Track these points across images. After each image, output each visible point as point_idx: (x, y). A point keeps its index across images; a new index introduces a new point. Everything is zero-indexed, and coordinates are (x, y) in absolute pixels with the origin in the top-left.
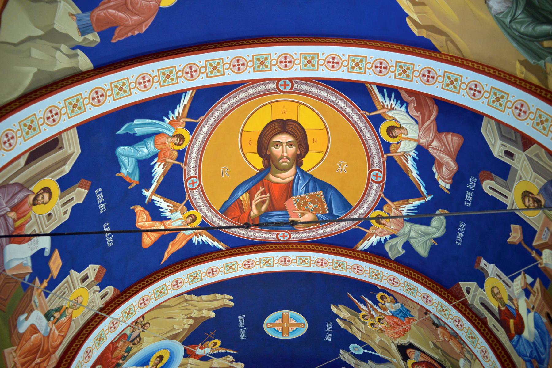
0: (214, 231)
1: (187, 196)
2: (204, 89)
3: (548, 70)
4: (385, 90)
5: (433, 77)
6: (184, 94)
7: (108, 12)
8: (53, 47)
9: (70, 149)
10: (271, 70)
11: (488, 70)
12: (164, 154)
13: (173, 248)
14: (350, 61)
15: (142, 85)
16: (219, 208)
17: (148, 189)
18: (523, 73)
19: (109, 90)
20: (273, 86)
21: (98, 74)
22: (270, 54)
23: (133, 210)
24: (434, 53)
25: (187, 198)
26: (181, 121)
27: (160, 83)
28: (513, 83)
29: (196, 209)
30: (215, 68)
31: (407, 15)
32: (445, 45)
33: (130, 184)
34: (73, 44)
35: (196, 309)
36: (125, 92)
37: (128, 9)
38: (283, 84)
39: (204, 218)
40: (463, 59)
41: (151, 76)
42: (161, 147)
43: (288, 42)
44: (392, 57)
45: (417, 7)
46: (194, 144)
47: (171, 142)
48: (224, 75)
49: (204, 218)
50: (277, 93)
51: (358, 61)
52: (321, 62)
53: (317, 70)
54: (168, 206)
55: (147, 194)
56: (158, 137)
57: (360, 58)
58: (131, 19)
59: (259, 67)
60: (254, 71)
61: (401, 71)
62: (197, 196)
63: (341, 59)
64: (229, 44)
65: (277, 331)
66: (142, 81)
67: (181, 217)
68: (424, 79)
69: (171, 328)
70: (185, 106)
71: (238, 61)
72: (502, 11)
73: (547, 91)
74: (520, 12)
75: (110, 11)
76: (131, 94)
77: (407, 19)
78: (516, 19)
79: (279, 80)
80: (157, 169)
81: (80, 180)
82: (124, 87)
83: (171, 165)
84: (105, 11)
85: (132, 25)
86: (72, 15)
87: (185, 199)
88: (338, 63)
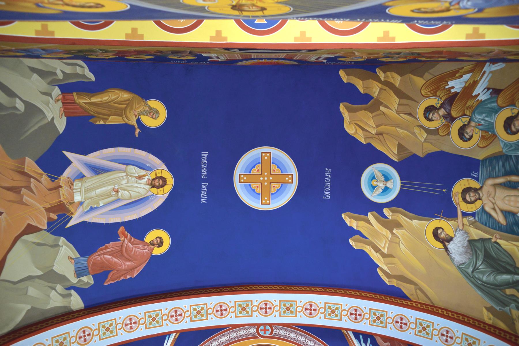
2: (186, 332)
3: (514, 317)
4: (361, 336)
5: (406, 324)
6: (168, 337)
7: (104, 257)
8: (49, 287)
10: (252, 316)
11: (457, 317)
14: (327, 308)
15: (129, 327)
18: (491, 319)
19: (96, 329)
20: (253, 330)
21: (88, 314)
22: (252, 301)
24: (405, 300)
27: (146, 325)
28: (482, 329)
30: (199, 313)
31: (378, 266)
32: (415, 293)
34: (68, 285)
36: (112, 332)
37: (122, 255)
38: (263, 329)
40: (433, 306)
41: (138, 318)
43: (268, 290)
44: (365, 305)
45: (385, 259)
48: (207, 319)
50: (257, 337)
51: (334, 309)
52: (299, 309)
53: (296, 316)
57: (336, 306)
58: (125, 265)
59: (240, 312)
60: (236, 317)
61: (375, 318)
63: (318, 307)
64: (213, 290)
65: (254, 190)
66: (128, 322)
68: (397, 326)
71: (221, 306)
72: (464, 262)
73: (516, 336)
74: (480, 263)
75: (105, 256)
76: (117, 335)
77: (378, 270)
78: (477, 269)
79: (259, 325)
82: (111, 328)
84: (102, 257)
86: (71, 258)
88: (315, 310)
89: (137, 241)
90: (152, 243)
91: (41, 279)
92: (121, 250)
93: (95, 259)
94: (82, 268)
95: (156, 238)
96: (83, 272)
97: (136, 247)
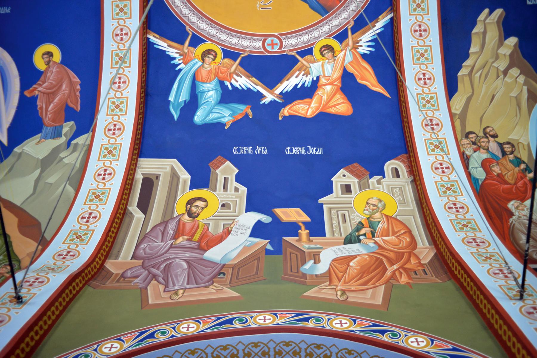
0: (360, 24)
1: (289, 53)
9: (166, 168)
12: (222, 73)
13: (368, 78)
16: (319, 16)
17: (261, 96)
23: (285, 117)
25: (293, 53)
26: (186, 51)
29: (313, 44)
33: (247, 115)
35: (493, 62)
37: (54, 92)
39: (329, 36)
42: (213, 75)
46: (219, 39)
47: (210, 64)
49: (329, 36)
54: (297, 77)
55: (269, 97)
56: (199, 78)
58: (65, 90)
62: (293, 41)
67: (321, 63)
69: (514, 102)
70: (169, 46)
75: (50, 109)
80: (239, 83)
81: (208, 167)
83: (239, 67)
84: (48, 113)
85: (70, 90)
86: (38, 142)
87: (294, 56)
89: (42, 78)
90: (48, 63)
91: (44, 171)
92: (48, 94)
93: (49, 120)
94: (53, 133)
95: (43, 58)
96: (58, 132)
97: (49, 79)
